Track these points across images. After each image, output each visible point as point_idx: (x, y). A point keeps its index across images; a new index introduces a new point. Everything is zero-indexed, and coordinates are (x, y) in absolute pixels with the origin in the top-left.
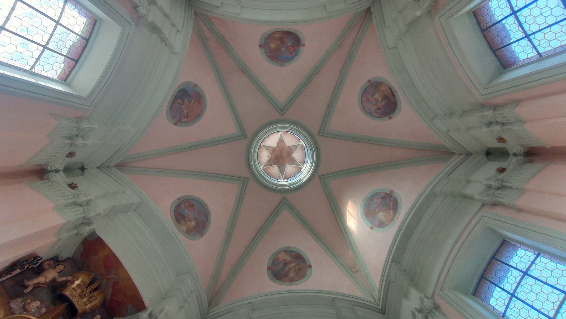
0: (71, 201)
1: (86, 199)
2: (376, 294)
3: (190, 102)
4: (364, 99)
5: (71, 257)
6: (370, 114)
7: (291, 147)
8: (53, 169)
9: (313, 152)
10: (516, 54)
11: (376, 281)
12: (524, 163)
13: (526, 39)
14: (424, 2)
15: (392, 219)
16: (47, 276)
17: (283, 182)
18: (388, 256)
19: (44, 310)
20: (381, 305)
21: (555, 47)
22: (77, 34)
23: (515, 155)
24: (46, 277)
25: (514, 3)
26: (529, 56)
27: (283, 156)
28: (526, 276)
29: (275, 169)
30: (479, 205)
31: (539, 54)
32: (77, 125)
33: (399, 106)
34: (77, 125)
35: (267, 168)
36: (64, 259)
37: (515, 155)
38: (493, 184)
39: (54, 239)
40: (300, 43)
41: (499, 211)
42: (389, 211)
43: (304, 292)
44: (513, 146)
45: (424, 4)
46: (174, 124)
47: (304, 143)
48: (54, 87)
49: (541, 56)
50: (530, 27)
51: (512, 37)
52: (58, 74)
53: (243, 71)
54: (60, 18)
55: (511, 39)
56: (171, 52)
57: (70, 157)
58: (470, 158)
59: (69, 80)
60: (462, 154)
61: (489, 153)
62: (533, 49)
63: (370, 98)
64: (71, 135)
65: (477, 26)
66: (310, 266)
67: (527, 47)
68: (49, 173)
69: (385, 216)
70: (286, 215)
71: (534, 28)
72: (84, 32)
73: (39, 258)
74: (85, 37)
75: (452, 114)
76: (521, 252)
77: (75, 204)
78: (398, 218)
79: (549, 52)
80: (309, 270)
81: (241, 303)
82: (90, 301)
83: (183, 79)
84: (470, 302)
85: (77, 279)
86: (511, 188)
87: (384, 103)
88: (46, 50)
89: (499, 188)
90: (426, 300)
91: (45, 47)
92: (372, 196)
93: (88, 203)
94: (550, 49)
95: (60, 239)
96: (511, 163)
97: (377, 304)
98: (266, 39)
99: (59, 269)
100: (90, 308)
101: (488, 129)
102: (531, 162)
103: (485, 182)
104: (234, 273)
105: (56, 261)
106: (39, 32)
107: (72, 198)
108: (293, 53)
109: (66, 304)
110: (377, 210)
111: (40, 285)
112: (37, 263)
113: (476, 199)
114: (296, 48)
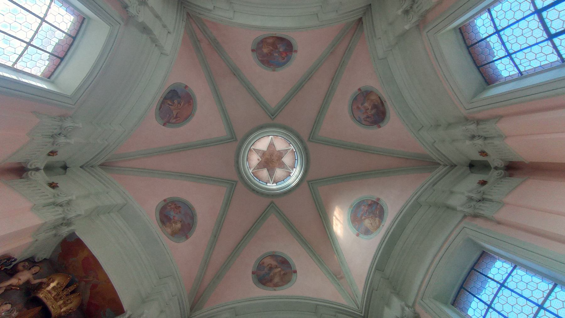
0: (51, 200)
1: (67, 199)
2: (359, 301)
3: (179, 103)
4: (355, 107)
5: (48, 258)
6: (360, 122)
7: (282, 151)
8: (33, 167)
9: (302, 155)
10: (499, 71)
11: (360, 287)
12: (505, 176)
13: (508, 57)
14: (413, 17)
15: (378, 227)
16: (21, 277)
17: (272, 186)
18: (372, 263)
19: (15, 314)
20: (363, 313)
21: (535, 67)
22: (63, 32)
23: (496, 168)
24: (20, 279)
25: (498, 22)
26: (511, 73)
27: (273, 159)
28: (503, 288)
29: (264, 173)
30: (460, 216)
31: (520, 72)
32: (60, 123)
33: (387, 115)
34: (60, 123)
35: (257, 171)
36: (40, 260)
37: (496, 168)
38: (474, 196)
39: (30, 240)
40: (292, 49)
41: (479, 222)
42: (375, 219)
43: (287, 298)
44: (495, 160)
45: (412, 19)
46: (163, 124)
47: (294, 149)
48: (36, 85)
49: (522, 75)
50: (512, 46)
51: (495, 54)
52: (42, 71)
53: (235, 74)
54: (46, 15)
55: (495, 56)
56: (161, 53)
57: (51, 155)
58: (454, 169)
59: (53, 78)
60: (447, 165)
61: (472, 166)
62: (515, 67)
63: (360, 106)
64: (54, 133)
65: (462, 42)
66: (295, 272)
67: (530, 53)
68: (29, 171)
69: (371, 224)
70: (273, 220)
71: (516, 48)
72: (71, 30)
73: (13, 260)
74: (72, 35)
75: (438, 126)
76: (498, 264)
77: (55, 204)
78: (383, 226)
79: (529, 71)
80: (294, 275)
81: (222, 308)
82: (65, 304)
83: (173, 80)
84: (448, 311)
85: (53, 281)
86: (491, 200)
87: (373, 112)
88: (30, 46)
89: (480, 200)
90: (407, 309)
91: (29, 44)
92: (359, 203)
93: (69, 203)
94: (531, 68)
95: (37, 240)
96: (491, 177)
97: (360, 311)
98: (259, 44)
99: (35, 271)
100: (65, 312)
101: (471, 142)
102: (511, 176)
103: (467, 194)
104: (218, 277)
105: (31, 262)
106: (24, 28)
107: (52, 198)
108: (285, 59)
109: (39, 309)
110: (363, 218)
111: (12, 287)
112: (10, 265)
113: (458, 210)
114: (288, 54)
